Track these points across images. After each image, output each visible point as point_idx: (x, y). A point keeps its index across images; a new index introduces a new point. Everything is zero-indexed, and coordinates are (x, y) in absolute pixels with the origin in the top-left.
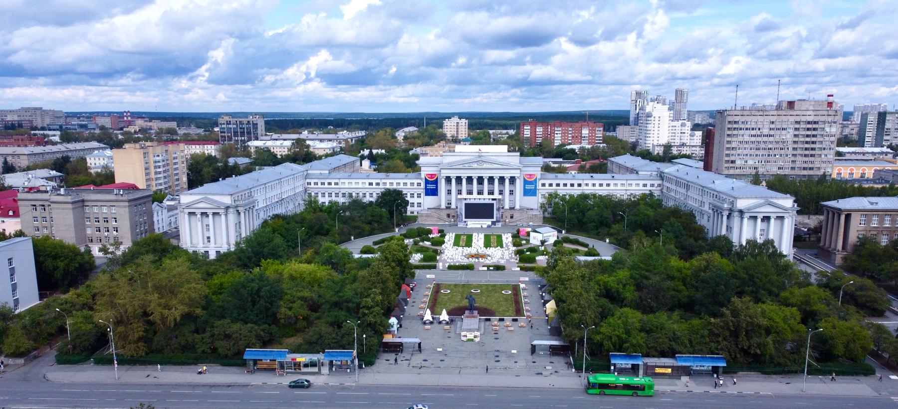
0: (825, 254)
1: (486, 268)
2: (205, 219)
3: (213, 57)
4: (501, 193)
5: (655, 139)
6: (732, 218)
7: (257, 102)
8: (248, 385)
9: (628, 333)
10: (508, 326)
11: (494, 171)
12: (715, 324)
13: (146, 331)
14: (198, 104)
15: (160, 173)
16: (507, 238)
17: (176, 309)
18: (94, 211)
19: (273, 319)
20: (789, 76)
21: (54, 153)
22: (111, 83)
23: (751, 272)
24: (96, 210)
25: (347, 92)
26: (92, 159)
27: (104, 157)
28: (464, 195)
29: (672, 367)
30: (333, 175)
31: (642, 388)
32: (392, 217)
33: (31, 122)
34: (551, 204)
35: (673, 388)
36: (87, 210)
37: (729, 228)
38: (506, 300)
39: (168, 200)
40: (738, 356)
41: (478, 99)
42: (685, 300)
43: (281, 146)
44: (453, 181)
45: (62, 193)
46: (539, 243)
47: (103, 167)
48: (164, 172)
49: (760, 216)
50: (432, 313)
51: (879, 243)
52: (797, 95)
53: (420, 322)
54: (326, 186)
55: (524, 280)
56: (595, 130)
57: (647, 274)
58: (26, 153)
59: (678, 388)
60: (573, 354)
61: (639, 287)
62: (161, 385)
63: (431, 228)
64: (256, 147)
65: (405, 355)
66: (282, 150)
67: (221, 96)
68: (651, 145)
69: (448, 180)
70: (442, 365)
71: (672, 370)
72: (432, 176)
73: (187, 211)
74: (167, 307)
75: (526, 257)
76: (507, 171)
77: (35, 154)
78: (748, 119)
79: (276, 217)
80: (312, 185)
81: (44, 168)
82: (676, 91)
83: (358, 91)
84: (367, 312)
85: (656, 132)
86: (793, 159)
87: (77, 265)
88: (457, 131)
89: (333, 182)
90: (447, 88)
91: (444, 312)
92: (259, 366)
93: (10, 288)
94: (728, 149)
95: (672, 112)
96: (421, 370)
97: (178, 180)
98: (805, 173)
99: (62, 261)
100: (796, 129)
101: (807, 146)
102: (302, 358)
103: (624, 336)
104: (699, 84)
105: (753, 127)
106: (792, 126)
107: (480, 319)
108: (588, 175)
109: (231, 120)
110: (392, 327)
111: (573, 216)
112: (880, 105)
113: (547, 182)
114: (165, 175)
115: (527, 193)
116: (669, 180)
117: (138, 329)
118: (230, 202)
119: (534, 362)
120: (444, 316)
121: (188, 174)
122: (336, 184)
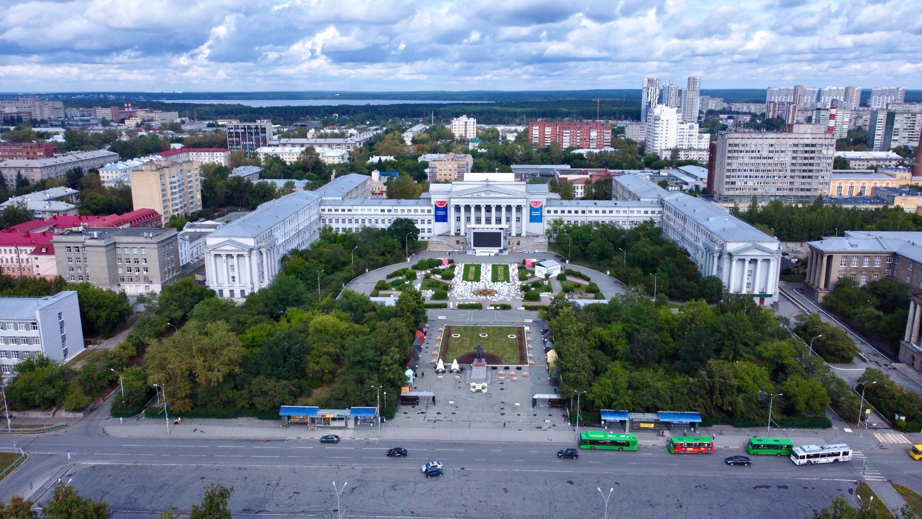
0: (809, 291)
1: (493, 308)
3: (214, 33)
4: (508, 220)
5: (664, 142)
6: (722, 260)
7: (259, 80)
9: (617, 392)
10: (513, 376)
11: (501, 200)
12: (693, 383)
14: (197, 82)
15: (175, 193)
16: (513, 270)
17: (219, 371)
18: (122, 252)
19: (303, 374)
20: (813, 52)
21: (65, 164)
22: (107, 60)
23: (731, 327)
24: (127, 251)
25: (353, 69)
26: (105, 172)
27: (117, 170)
28: (473, 224)
30: (347, 201)
31: (627, 444)
32: (404, 246)
33: (30, 113)
34: (556, 230)
36: (119, 251)
37: (719, 269)
38: (511, 345)
39: (188, 227)
40: (713, 412)
41: (489, 76)
42: (671, 352)
43: (290, 153)
44: (462, 210)
45: (95, 236)
46: (543, 277)
47: (117, 182)
48: (180, 191)
49: (748, 259)
50: (444, 361)
51: (855, 283)
52: (820, 71)
53: (433, 370)
54: (340, 212)
55: (528, 322)
56: (603, 133)
57: (638, 327)
60: (569, 408)
61: (630, 338)
64: (265, 154)
65: (421, 407)
66: (291, 156)
67: (222, 74)
68: (659, 149)
69: (458, 208)
72: (442, 203)
74: (211, 369)
75: (531, 292)
76: (513, 200)
77: (47, 167)
78: (748, 141)
79: (295, 252)
80: (327, 212)
81: (60, 186)
82: (689, 79)
83: (365, 68)
84: (386, 369)
85: (664, 136)
86: (791, 180)
87: (117, 314)
88: (466, 131)
89: (346, 208)
90: (457, 65)
91: (455, 361)
92: (292, 420)
93: (60, 340)
94: (728, 170)
95: (680, 114)
97: (192, 197)
98: (803, 193)
99: (104, 311)
100: (794, 152)
101: (805, 168)
102: (330, 414)
103: (613, 395)
104: (720, 60)
105: (753, 149)
106: (790, 149)
108: (592, 202)
110: (409, 379)
112: (898, 89)
113: (552, 209)
114: (181, 194)
115: (533, 219)
116: (669, 209)
117: (184, 388)
119: (535, 415)
120: (455, 366)
121: (202, 191)
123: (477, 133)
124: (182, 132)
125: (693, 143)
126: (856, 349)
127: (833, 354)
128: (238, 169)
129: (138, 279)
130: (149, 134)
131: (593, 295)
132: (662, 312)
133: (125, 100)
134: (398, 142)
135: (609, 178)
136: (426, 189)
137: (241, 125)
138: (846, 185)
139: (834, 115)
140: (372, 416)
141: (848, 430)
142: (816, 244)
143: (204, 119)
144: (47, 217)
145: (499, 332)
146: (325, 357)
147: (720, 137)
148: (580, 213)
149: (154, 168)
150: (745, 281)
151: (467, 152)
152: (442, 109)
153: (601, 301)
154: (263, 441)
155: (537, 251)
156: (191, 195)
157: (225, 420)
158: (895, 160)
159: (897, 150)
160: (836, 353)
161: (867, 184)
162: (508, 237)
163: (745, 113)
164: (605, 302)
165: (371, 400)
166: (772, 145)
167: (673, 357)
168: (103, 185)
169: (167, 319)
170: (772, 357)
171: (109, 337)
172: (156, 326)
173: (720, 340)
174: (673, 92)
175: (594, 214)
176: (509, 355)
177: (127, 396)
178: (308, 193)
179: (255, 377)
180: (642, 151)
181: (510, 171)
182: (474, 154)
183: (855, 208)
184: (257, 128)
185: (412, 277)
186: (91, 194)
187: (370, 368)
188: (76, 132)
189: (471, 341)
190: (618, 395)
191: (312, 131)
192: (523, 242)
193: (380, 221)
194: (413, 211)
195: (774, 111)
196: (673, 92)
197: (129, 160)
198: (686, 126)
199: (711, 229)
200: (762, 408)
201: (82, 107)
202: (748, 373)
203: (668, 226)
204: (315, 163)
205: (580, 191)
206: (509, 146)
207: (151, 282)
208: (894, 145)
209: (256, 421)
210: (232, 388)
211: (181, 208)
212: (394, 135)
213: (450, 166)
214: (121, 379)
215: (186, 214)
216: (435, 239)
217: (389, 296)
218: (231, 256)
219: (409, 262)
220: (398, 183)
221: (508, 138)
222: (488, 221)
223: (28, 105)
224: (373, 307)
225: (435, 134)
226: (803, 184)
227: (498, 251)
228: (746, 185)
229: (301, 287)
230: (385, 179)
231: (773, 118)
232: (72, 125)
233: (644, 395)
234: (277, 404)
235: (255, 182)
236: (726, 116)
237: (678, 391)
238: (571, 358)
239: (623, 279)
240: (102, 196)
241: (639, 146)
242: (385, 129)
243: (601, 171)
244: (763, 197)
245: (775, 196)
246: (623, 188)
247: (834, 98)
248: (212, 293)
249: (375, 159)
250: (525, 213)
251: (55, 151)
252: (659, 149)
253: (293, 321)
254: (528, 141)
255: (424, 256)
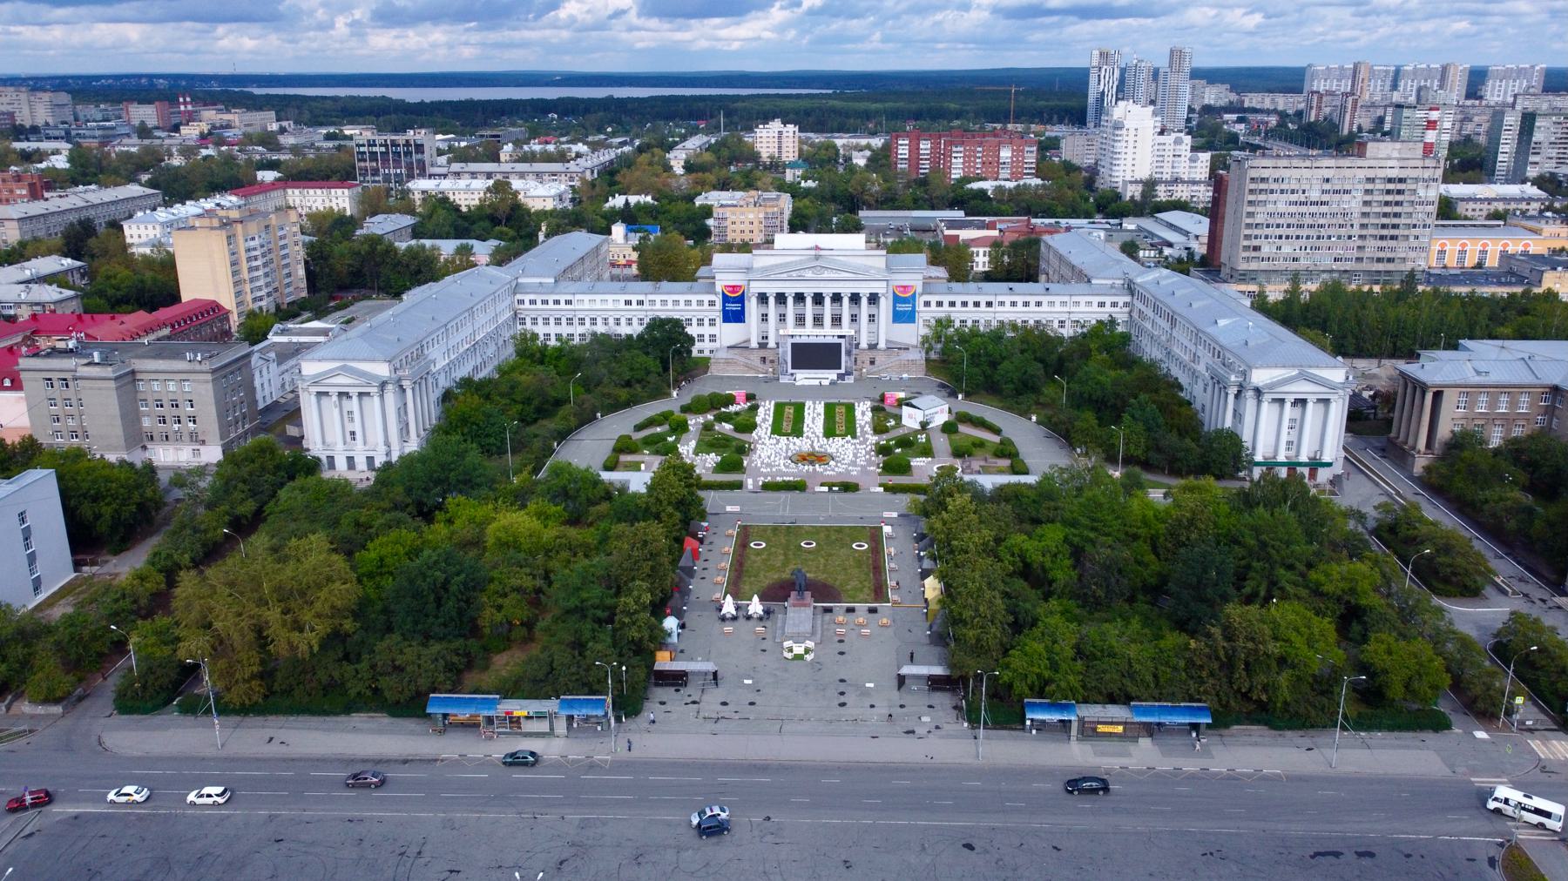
0: (1398, 454)
1: (826, 489)
2: (345, 401)
4: (854, 318)
5: (1129, 168)
8: (436, 760)
9: (1054, 667)
10: (861, 626)
11: (841, 284)
13: (263, 662)
15: (257, 268)
16: (863, 414)
17: (312, 630)
19: (475, 631)
21: (64, 212)
23: (1264, 537)
24: (156, 386)
28: (790, 328)
29: (1125, 724)
32: (666, 369)
35: (1124, 761)
36: (141, 386)
37: (1238, 415)
39: (276, 334)
40: (1232, 703)
42: (1153, 581)
43: (468, 189)
45: (97, 360)
46: (918, 427)
47: (154, 246)
48: (265, 265)
49: (1290, 398)
50: (735, 597)
51: (1484, 442)
53: (715, 615)
54: (551, 306)
55: (889, 515)
56: (1022, 151)
57: (1092, 535)
58: (15, 216)
59: (1133, 761)
61: (1077, 554)
62: (293, 760)
63: (733, 393)
64: (423, 192)
65: (692, 691)
69: (763, 298)
70: (751, 713)
71: (1125, 729)
72: (734, 288)
73: (314, 389)
77: (31, 218)
78: (1286, 173)
79: (467, 383)
80: (527, 305)
82: (1172, 52)
85: (1130, 156)
86: (1360, 243)
87: (133, 508)
88: (780, 148)
89: (563, 298)
91: (756, 598)
94: (1249, 226)
95: (1159, 119)
96: (718, 725)
97: (289, 275)
98: (1381, 267)
99: (108, 504)
101: (1385, 221)
102: (520, 708)
103: (1047, 674)
106: (1360, 187)
107: (815, 607)
109: (376, 137)
110: (670, 635)
111: (976, 370)
112: (1533, 67)
113: (933, 299)
114: (267, 270)
115: (898, 317)
116: (1143, 299)
117: (250, 663)
118: (388, 374)
120: (756, 607)
121: (306, 263)
122: (568, 302)
123: (800, 150)
124: (278, 148)
125: (1181, 170)
126: (1490, 571)
127: (1446, 581)
128: (373, 219)
129: (179, 437)
130: (220, 153)
131: (1006, 463)
132: (1135, 504)
133: (184, 88)
134: (659, 169)
135: (1034, 236)
136: (707, 261)
137: (380, 139)
138: (1453, 248)
139: (1435, 122)
140: (600, 713)
141: (1481, 735)
142: (1412, 369)
143: (321, 124)
144: (24, 314)
145: (836, 537)
146: (514, 595)
147: (1234, 166)
148: (983, 306)
149: (216, 223)
150: (1284, 438)
151: (782, 187)
152: (739, 105)
153: (1023, 479)
154: (396, 761)
155: (905, 376)
156: (286, 271)
157: (327, 719)
158: (1538, 200)
159: (1539, 182)
160: (1454, 579)
161: (1491, 247)
162: (854, 351)
163: (1268, 112)
164: (1030, 479)
165: (599, 682)
166: (1328, 180)
167: (1156, 590)
168: (130, 251)
169: (227, 518)
170: (1339, 592)
171: (121, 551)
172: (206, 531)
173: (1243, 558)
174: (1144, 75)
175: (1008, 307)
176: (854, 583)
177: (143, 676)
178: (494, 271)
179: (382, 639)
180: (1090, 184)
181: (856, 228)
182: (795, 192)
183: (1473, 292)
184: (407, 144)
185: (680, 428)
186: (104, 269)
187: (599, 621)
188: (90, 149)
189: (785, 555)
190: (1057, 671)
191: (509, 148)
192: (880, 359)
193: (623, 321)
194: (682, 303)
195: (1319, 108)
196: (1144, 75)
197: (178, 205)
198: (1168, 139)
199: (1223, 341)
200: (1323, 693)
201: (106, 101)
202: (1297, 630)
203: (1141, 330)
204: (512, 209)
205: (981, 262)
206: (858, 176)
207: (203, 442)
208: (1532, 172)
209: (385, 720)
210: (340, 660)
211: (269, 294)
212: (653, 155)
213: (751, 216)
214: (134, 639)
215: (278, 307)
216: (723, 355)
217: (635, 467)
218: (347, 395)
219: (675, 400)
220: (658, 248)
221: (854, 161)
222: (818, 321)
223: (7, 100)
224: (608, 493)
225: (725, 153)
226: (1381, 249)
227: (835, 377)
228: (1280, 251)
229: (474, 456)
230: (635, 239)
231: (1317, 121)
232: (85, 137)
233: (1104, 672)
234: (423, 689)
235: (402, 246)
236: (1234, 117)
237: (1167, 664)
238: (970, 601)
239: (1063, 433)
240: (127, 272)
241: (1084, 174)
242: (637, 142)
243: (1018, 221)
244: (1310, 274)
245: (1331, 271)
246: (1061, 258)
247: (1422, 83)
248: (313, 466)
249: (618, 201)
250: (885, 306)
251: (49, 187)
252: (1120, 180)
253: (458, 523)
254: (889, 166)
255: (702, 388)
